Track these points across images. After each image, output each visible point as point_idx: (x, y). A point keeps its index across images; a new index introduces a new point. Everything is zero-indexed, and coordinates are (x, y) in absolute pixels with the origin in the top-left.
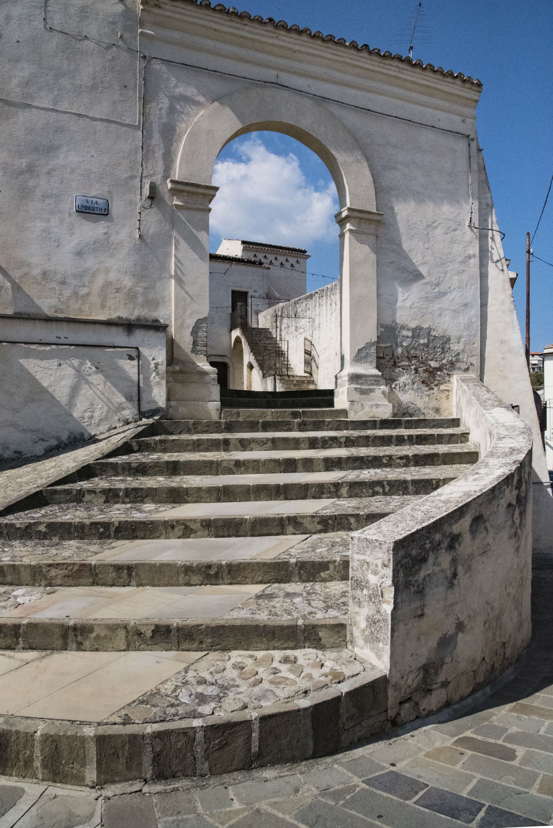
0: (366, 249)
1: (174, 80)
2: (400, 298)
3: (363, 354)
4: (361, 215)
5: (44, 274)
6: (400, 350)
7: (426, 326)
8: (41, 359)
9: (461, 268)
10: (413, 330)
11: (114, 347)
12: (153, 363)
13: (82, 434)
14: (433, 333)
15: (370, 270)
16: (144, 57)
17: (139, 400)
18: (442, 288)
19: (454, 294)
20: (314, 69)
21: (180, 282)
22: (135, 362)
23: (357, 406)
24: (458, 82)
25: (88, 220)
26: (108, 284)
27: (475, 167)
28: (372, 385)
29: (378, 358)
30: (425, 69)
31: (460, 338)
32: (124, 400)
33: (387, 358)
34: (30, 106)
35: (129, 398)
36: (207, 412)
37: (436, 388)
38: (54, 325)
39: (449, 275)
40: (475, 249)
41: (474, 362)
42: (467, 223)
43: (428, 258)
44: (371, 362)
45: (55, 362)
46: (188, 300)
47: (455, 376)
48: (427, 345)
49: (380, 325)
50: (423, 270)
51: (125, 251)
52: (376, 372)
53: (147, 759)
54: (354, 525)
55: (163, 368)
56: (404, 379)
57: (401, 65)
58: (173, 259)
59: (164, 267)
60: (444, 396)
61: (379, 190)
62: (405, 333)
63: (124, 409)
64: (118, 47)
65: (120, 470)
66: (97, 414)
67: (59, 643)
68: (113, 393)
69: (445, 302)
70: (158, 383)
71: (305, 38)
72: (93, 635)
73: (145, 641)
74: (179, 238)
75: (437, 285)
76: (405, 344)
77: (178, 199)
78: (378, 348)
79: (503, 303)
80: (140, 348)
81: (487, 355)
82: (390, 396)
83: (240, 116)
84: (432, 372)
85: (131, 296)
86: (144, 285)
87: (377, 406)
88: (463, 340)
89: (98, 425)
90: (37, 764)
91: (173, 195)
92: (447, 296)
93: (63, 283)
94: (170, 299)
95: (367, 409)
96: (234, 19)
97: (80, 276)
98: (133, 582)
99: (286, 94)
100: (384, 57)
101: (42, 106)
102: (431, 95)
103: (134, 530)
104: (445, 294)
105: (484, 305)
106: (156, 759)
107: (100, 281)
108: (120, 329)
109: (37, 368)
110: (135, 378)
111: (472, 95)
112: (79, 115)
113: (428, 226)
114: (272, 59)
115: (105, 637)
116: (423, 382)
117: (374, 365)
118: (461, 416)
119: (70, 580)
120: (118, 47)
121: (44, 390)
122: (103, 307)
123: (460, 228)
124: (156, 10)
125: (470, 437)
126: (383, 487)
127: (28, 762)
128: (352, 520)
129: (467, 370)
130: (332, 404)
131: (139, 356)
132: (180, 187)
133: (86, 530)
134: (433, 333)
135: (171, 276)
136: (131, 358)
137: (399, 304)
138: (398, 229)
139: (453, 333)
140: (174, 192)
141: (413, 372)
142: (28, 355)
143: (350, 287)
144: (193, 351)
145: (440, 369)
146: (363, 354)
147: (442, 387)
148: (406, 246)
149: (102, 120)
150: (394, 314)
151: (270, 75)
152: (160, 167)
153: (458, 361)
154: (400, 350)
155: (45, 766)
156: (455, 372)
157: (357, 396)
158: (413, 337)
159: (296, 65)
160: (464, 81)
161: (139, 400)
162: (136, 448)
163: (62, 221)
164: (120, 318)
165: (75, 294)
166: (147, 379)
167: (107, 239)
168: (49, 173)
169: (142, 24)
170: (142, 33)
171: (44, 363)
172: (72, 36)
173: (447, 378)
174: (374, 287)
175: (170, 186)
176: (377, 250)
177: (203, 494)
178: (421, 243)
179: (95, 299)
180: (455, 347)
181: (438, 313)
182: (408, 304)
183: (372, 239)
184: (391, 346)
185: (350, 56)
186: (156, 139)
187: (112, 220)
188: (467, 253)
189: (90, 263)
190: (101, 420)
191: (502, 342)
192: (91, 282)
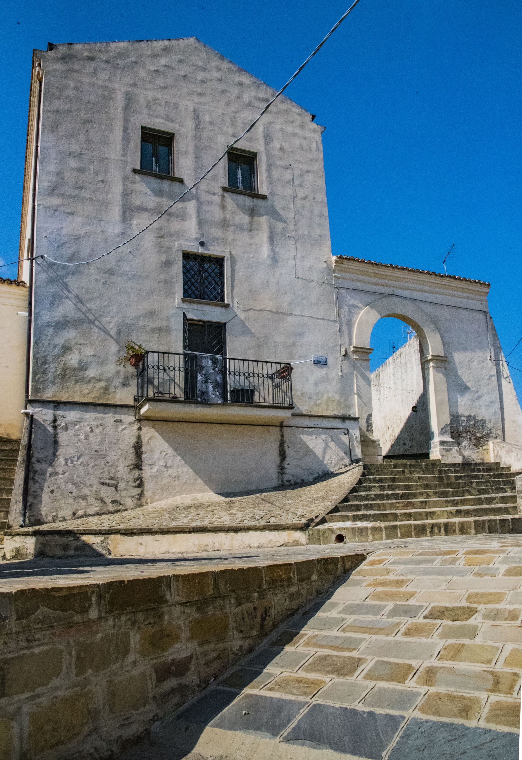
0: (441, 375)
1: (349, 297)
2: (459, 400)
3: (444, 431)
4: (438, 358)
5: (302, 394)
6: (461, 428)
7: (473, 415)
8: (309, 435)
9: (488, 382)
10: (467, 417)
11: (338, 429)
12: (354, 436)
13: (328, 471)
14: (477, 418)
15: (444, 386)
16: (337, 288)
17: (351, 455)
18: (479, 394)
19: (486, 396)
20: (411, 285)
21: (359, 396)
22: (347, 436)
23: (445, 458)
24: (478, 284)
25: (319, 367)
26: (329, 398)
27: (490, 327)
28: (451, 446)
29: (451, 432)
30: (462, 280)
31: (491, 420)
32: (344, 455)
33: (455, 432)
34: (292, 314)
35: (346, 454)
36: (377, 461)
37: (481, 448)
38: (313, 418)
39: (482, 387)
40: (494, 372)
41: (499, 433)
42: (489, 358)
43: (471, 378)
44: (448, 435)
45: (314, 437)
46: (363, 405)
47: (490, 441)
48: (474, 425)
49: (451, 415)
50: (469, 385)
51: (335, 381)
52: (451, 440)
53: (487, 527)
54: (491, 492)
55: (359, 439)
56: (464, 443)
57: (450, 279)
58: (355, 385)
59: (352, 390)
60: (485, 452)
61: (444, 344)
62: (463, 419)
63: (344, 459)
64: (325, 283)
65: (372, 481)
66: (333, 462)
67: (425, 517)
68: (339, 451)
69: (481, 401)
70: (358, 446)
71: (406, 271)
72: (436, 514)
73: (453, 515)
74: (357, 374)
75: (477, 392)
76: (463, 425)
77: (356, 356)
78: (451, 427)
79: (512, 400)
80: (349, 430)
81: (506, 429)
82: (461, 454)
83: (379, 313)
84: (478, 439)
85: (339, 404)
86: (344, 398)
87: (455, 457)
88: (493, 421)
89: (334, 467)
90: (457, 531)
91: (354, 353)
92: (482, 399)
93: (310, 398)
94: (355, 405)
95: (450, 459)
96: (374, 266)
97: (317, 394)
98: (427, 507)
99: (397, 299)
100: (442, 276)
101: (297, 314)
102: (464, 292)
103: (408, 496)
104: (481, 397)
105: (501, 402)
106: (489, 527)
107: (325, 397)
108: (340, 420)
109: (307, 440)
110: (348, 444)
111: (485, 290)
112: (312, 317)
113: (469, 361)
114: (390, 282)
115: (440, 515)
116: (474, 445)
117: (450, 436)
118: (501, 460)
119: (404, 508)
120: (325, 283)
121: (311, 450)
122: (327, 410)
123: (485, 361)
124: (341, 265)
125: (511, 469)
126: (490, 483)
127: (454, 531)
128: (490, 490)
129: (496, 438)
130: (429, 458)
131: (348, 433)
132: (357, 349)
133: (390, 497)
134: (477, 418)
135: (355, 394)
136: (345, 434)
137: (459, 403)
138: (455, 363)
139: (487, 418)
140: (354, 352)
141: (469, 439)
142: (303, 433)
143: (435, 395)
144: (367, 431)
145: (482, 438)
146: (444, 431)
147: (484, 447)
148: (459, 373)
149: (322, 319)
150: (457, 408)
151: (389, 290)
152: (347, 340)
153: (491, 433)
154: (461, 428)
155: (459, 531)
156: (490, 439)
157: (444, 453)
158: (467, 421)
159: (402, 284)
160: (482, 284)
161: (351, 455)
162: (367, 474)
163: (308, 368)
164: (335, 415)
165: (315, 403)
166: (353, 444)
167: (327, 376)
168: (301, 346)
169: (334, 271)
170: (335, 276)
171: (310, 437)
172: (307, 280)
173: (486, 443)
174: (447, 395)
175: (352, 349)
176: (446, 376)
177: (418, 487)
178: (467, 371)
179: (324, 406)
180: (489, 425)
181: (478, 407)
182: (463, 403)
183: (443, 370)
184: (457, 426)
185: (427, 278)
186: (345, 327)
187: (329, 367)
188: (490, 374)
189: (321, 388)
190: (335, 465)
191: (514, 422)
192: (322, 397)
